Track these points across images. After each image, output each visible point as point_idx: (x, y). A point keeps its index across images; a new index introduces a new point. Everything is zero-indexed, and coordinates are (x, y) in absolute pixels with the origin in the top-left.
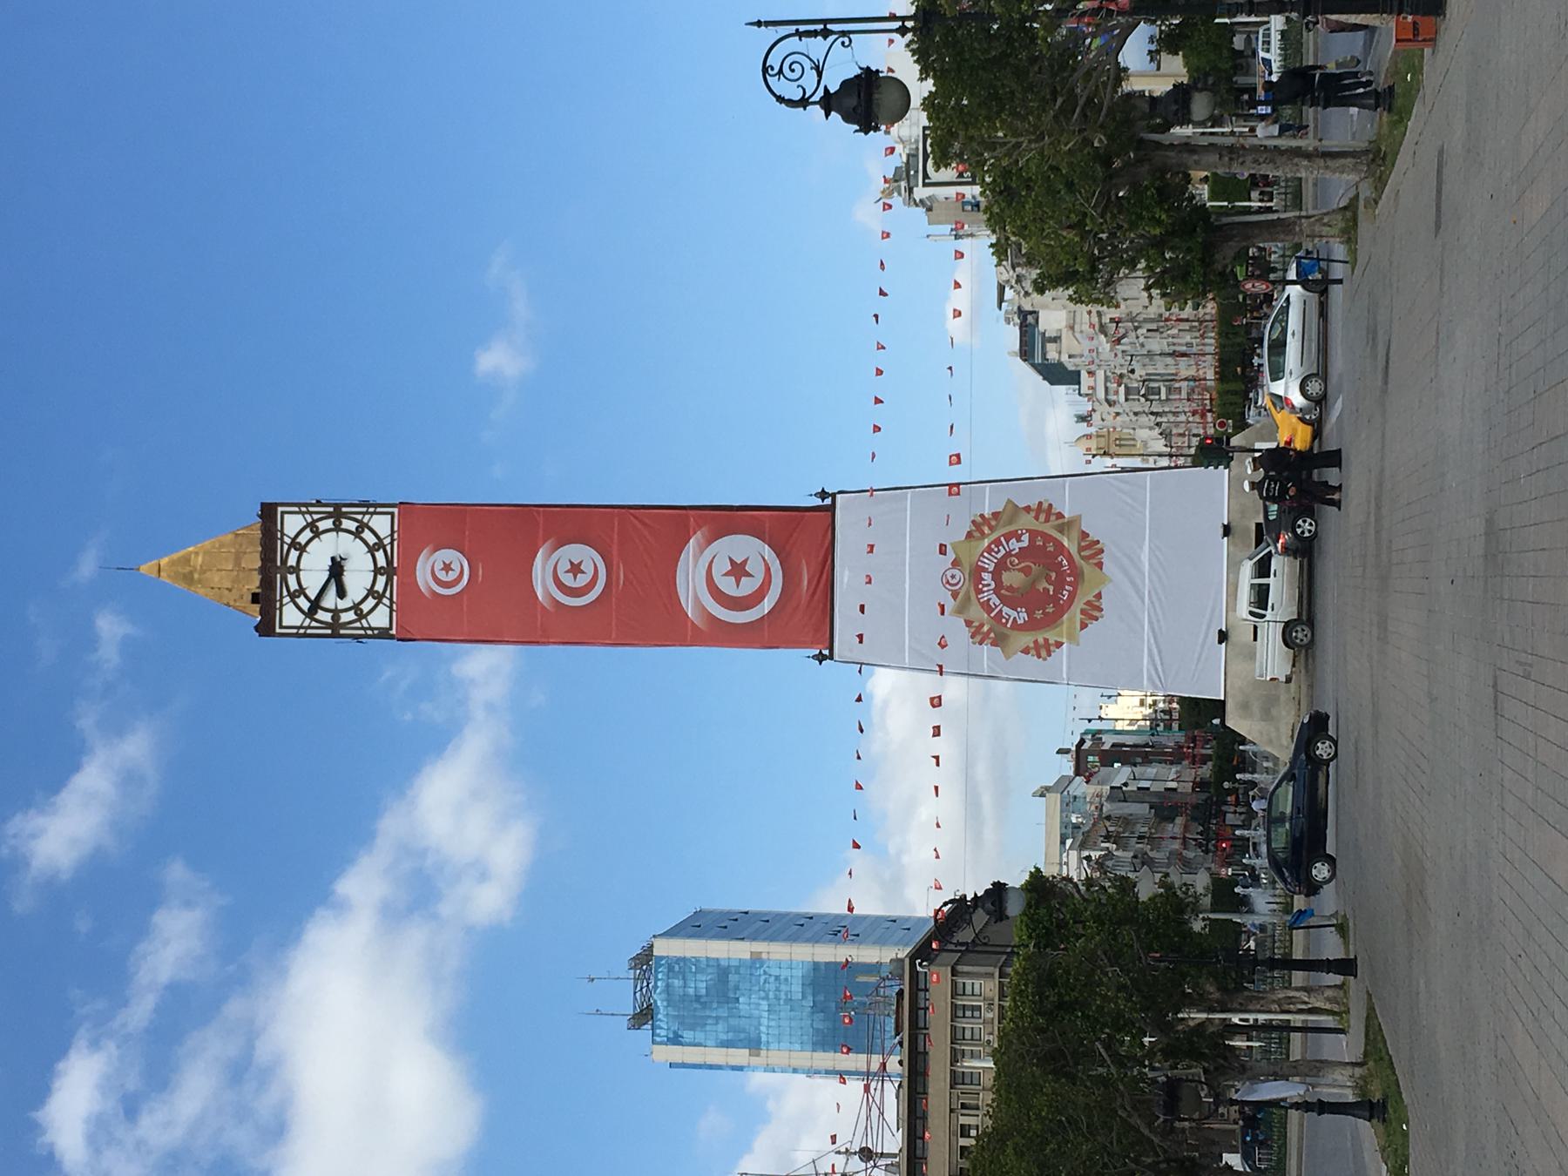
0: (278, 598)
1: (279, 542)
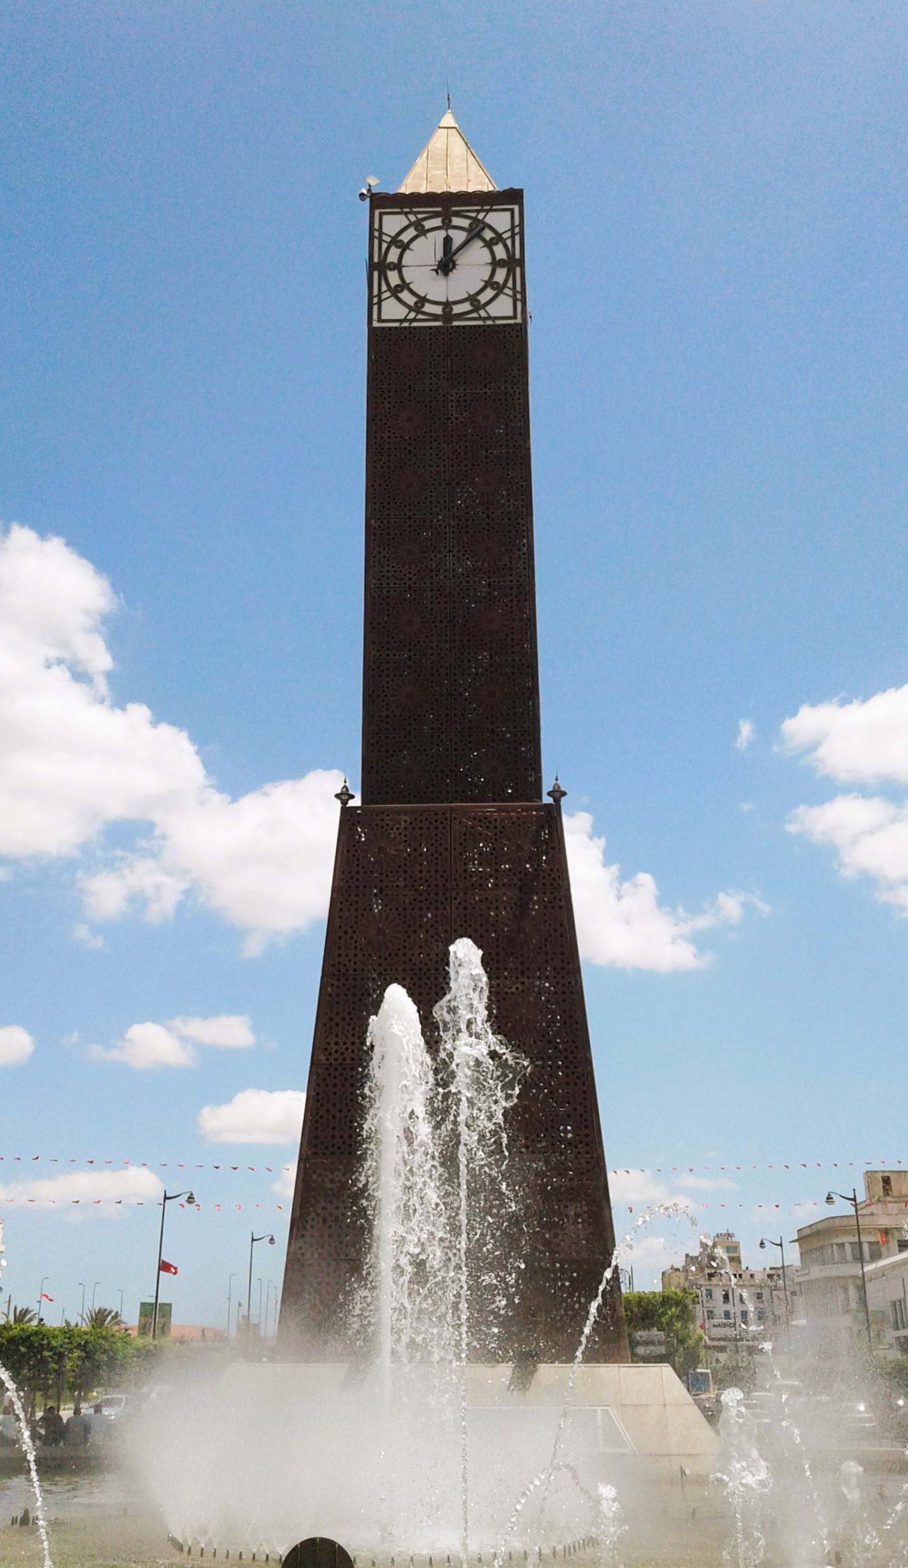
0: (414, 210)
1: (414, 324)
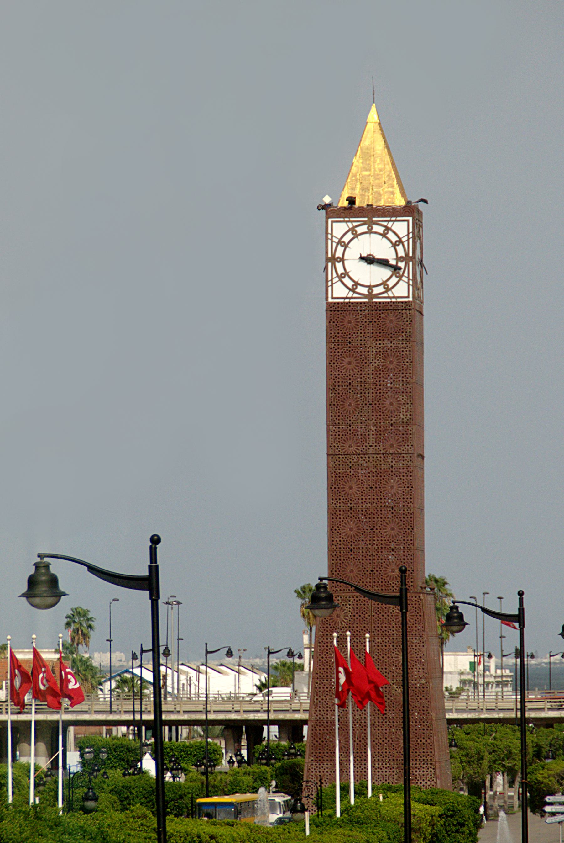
1: (352, 300)
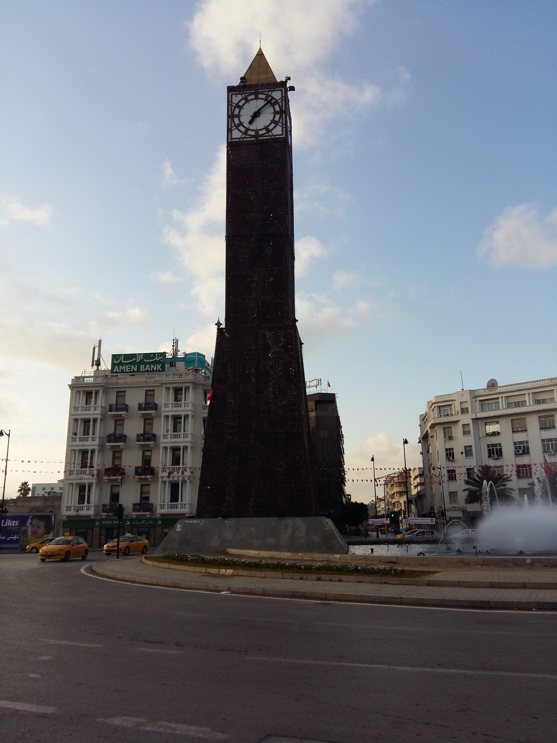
1: (245, 140)
